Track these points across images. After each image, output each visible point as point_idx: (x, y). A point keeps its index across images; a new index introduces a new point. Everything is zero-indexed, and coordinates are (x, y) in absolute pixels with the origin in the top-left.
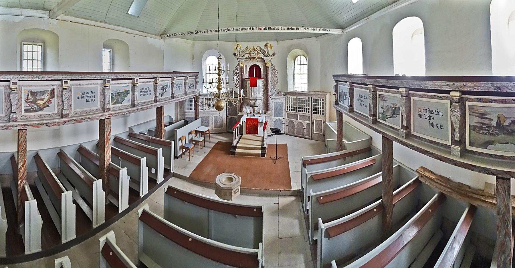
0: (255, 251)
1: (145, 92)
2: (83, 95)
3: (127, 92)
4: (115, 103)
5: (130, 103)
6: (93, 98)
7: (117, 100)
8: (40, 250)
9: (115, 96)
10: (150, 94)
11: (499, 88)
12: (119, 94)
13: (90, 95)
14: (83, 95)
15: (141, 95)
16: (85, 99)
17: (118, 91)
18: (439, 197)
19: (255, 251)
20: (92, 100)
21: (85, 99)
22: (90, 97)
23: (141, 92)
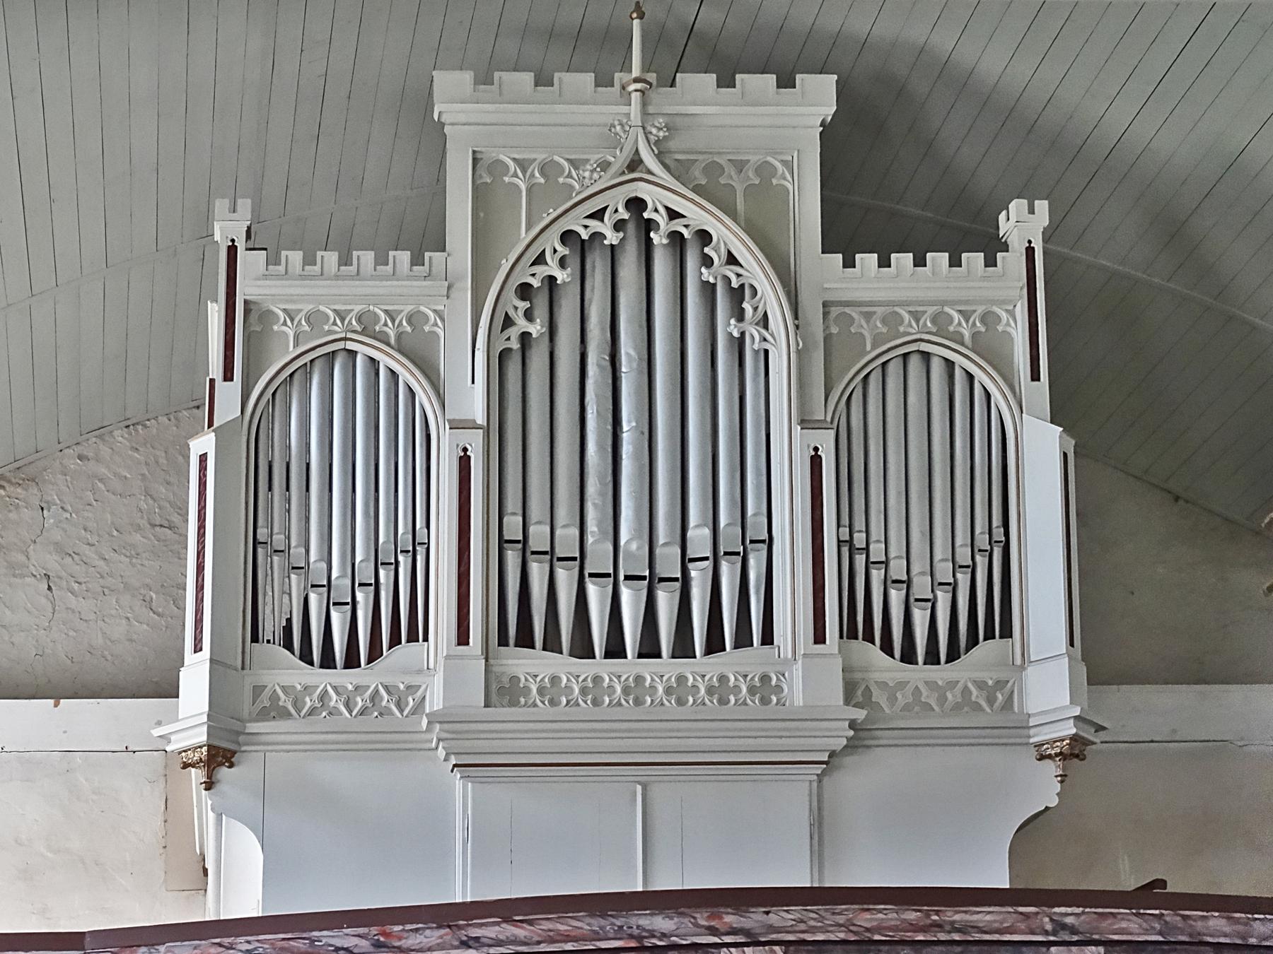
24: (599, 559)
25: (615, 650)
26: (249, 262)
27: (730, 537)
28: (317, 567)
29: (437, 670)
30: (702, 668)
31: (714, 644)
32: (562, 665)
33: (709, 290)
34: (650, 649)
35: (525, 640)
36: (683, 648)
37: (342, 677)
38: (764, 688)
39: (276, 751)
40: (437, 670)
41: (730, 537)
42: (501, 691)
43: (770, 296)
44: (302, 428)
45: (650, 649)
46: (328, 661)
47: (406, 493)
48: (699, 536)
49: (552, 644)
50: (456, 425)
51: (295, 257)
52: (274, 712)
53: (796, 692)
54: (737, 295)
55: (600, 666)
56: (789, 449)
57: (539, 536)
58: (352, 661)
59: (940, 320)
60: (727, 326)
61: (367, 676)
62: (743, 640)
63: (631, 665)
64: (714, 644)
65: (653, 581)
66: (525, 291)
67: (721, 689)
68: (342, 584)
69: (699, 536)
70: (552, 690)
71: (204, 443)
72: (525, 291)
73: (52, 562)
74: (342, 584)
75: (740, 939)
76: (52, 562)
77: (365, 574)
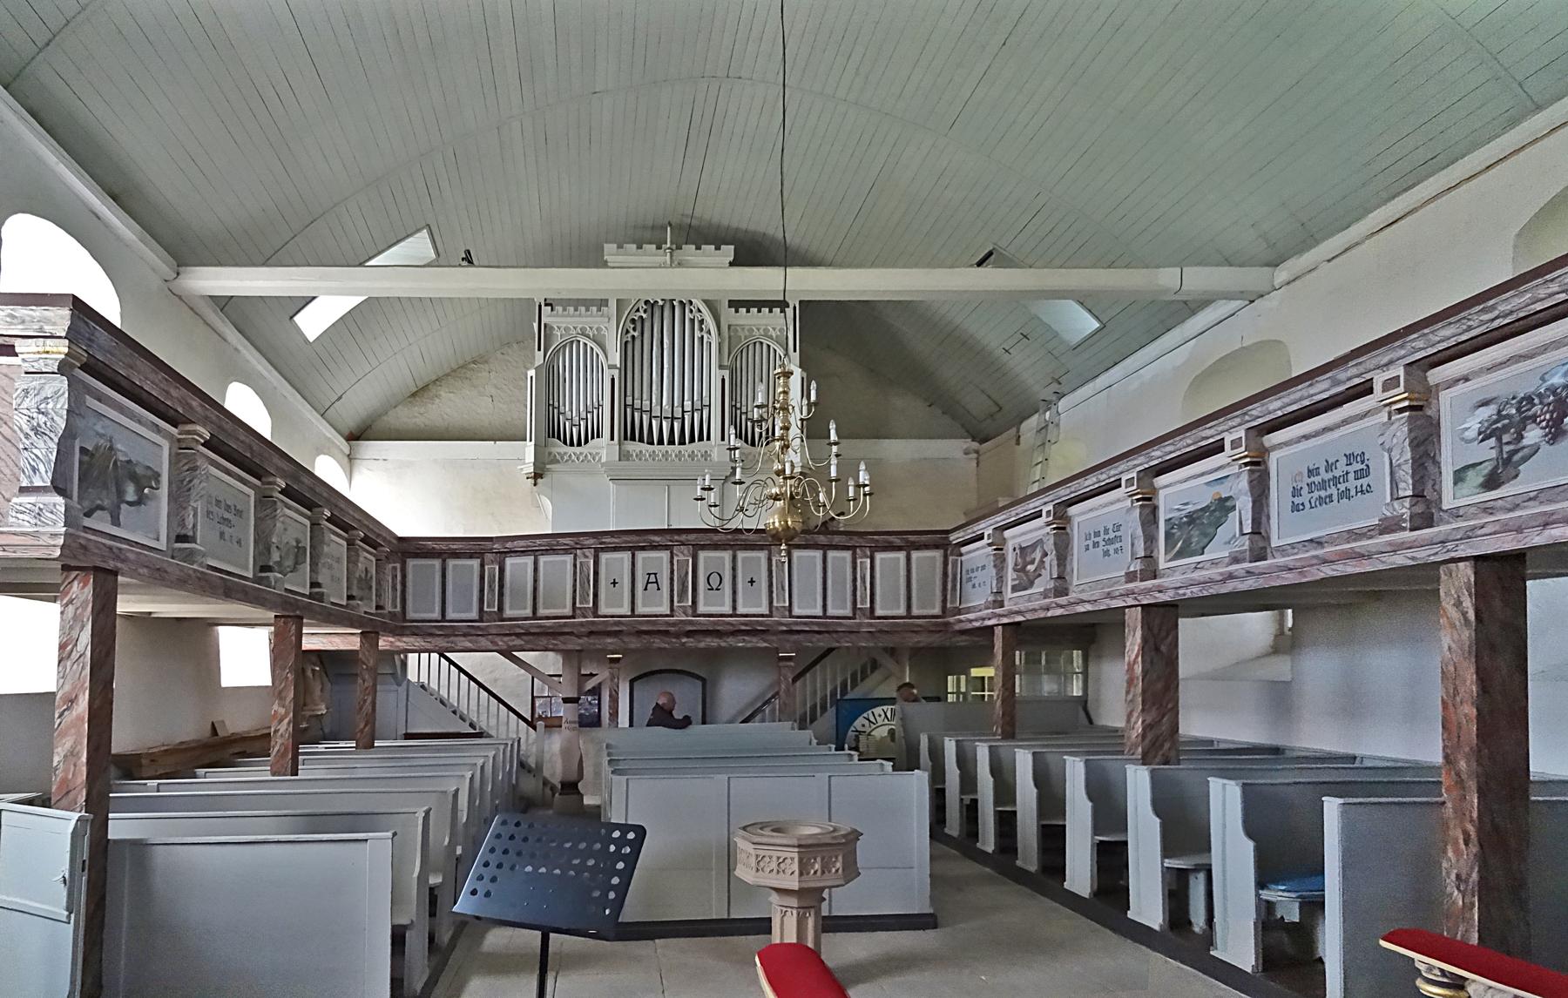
0: (998, 631)
1: (1323, 485)
2: (1297, 500)
3: (1223, 506)
4: (1180, 555)
5: (1245, 544)
6: (1118, 545)
7: (1187, 543)
8: (224, 685)
9: (1180, 526)
10: (1367, 490)
11: (1413, 558)
12: (1192, 519)
13: (1112, 535)
14: (1297, 500)
15: (1296, 508)
16: (1099, 550)
17: (1190, 508)
18: (1147, 625)
19: (998, 631)
20: (1116, 551)
21: (1099, 550)
22: (1110, 542)
23: (1296, 492)
24: (656, 412)
25: (661, 442)
26: (546, 310)
27: (698, 405)
28: (568, 414)
29: (604, 448)
30: (688, 447)
31: (692, 440)
32: (644, 447)
33: (692, 321)
34: (671, 442)
35: (633, 439)
36: (682, 442)
37: (577, 450)
38: (706, 455)
39: (556, 472)
40: (604, 448)
41: (698, 405)
42: (624, 456)
43: (710, 322)
44: (563, 362)
45: (671, 442)
46: (572, 444)
47: (590, 393)
48: (688, 404)
49: (641, 440)
50: (610, 367)
51: (559, 309)
52: (555, 461)
53: (715, 456)
54: (701, 322)
55: (656, 447)
56: (717, 375)
57: (637, 404)
58: (579, 444)
59: (766, 330)
60: (697, 334)
61: (584, 449)
62: (701, 439)
63: (666, 447)
64: (692, 440)
65: (673, 418)
66: (633, 321)
67: (692, 455)
68: (576, 419)
69: (688, 404)
70: (640, 455)
71: (532, 373)
72: (633, 321)
73: (493, 391)
74: (576, 419)
75: (1497, 528)
76: (493, 391)
77: (583, 415)
